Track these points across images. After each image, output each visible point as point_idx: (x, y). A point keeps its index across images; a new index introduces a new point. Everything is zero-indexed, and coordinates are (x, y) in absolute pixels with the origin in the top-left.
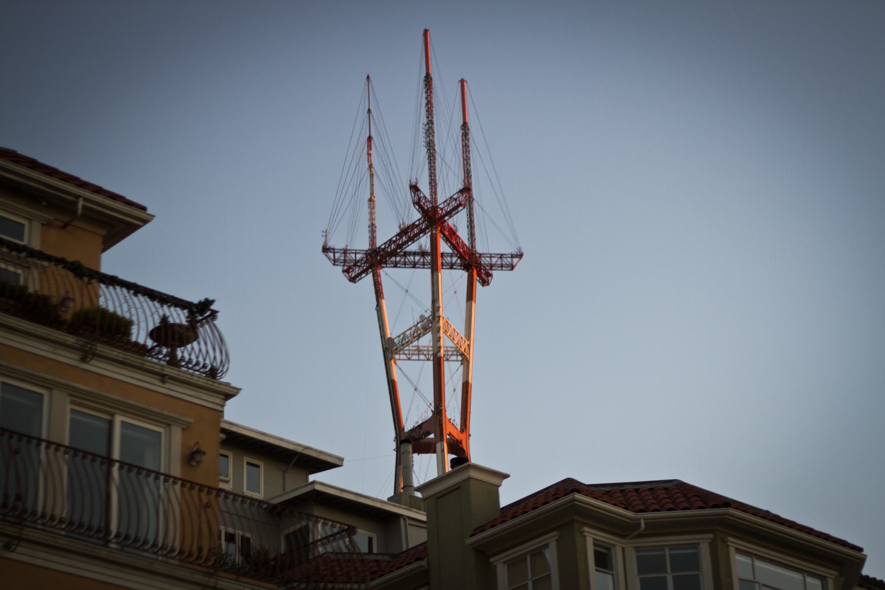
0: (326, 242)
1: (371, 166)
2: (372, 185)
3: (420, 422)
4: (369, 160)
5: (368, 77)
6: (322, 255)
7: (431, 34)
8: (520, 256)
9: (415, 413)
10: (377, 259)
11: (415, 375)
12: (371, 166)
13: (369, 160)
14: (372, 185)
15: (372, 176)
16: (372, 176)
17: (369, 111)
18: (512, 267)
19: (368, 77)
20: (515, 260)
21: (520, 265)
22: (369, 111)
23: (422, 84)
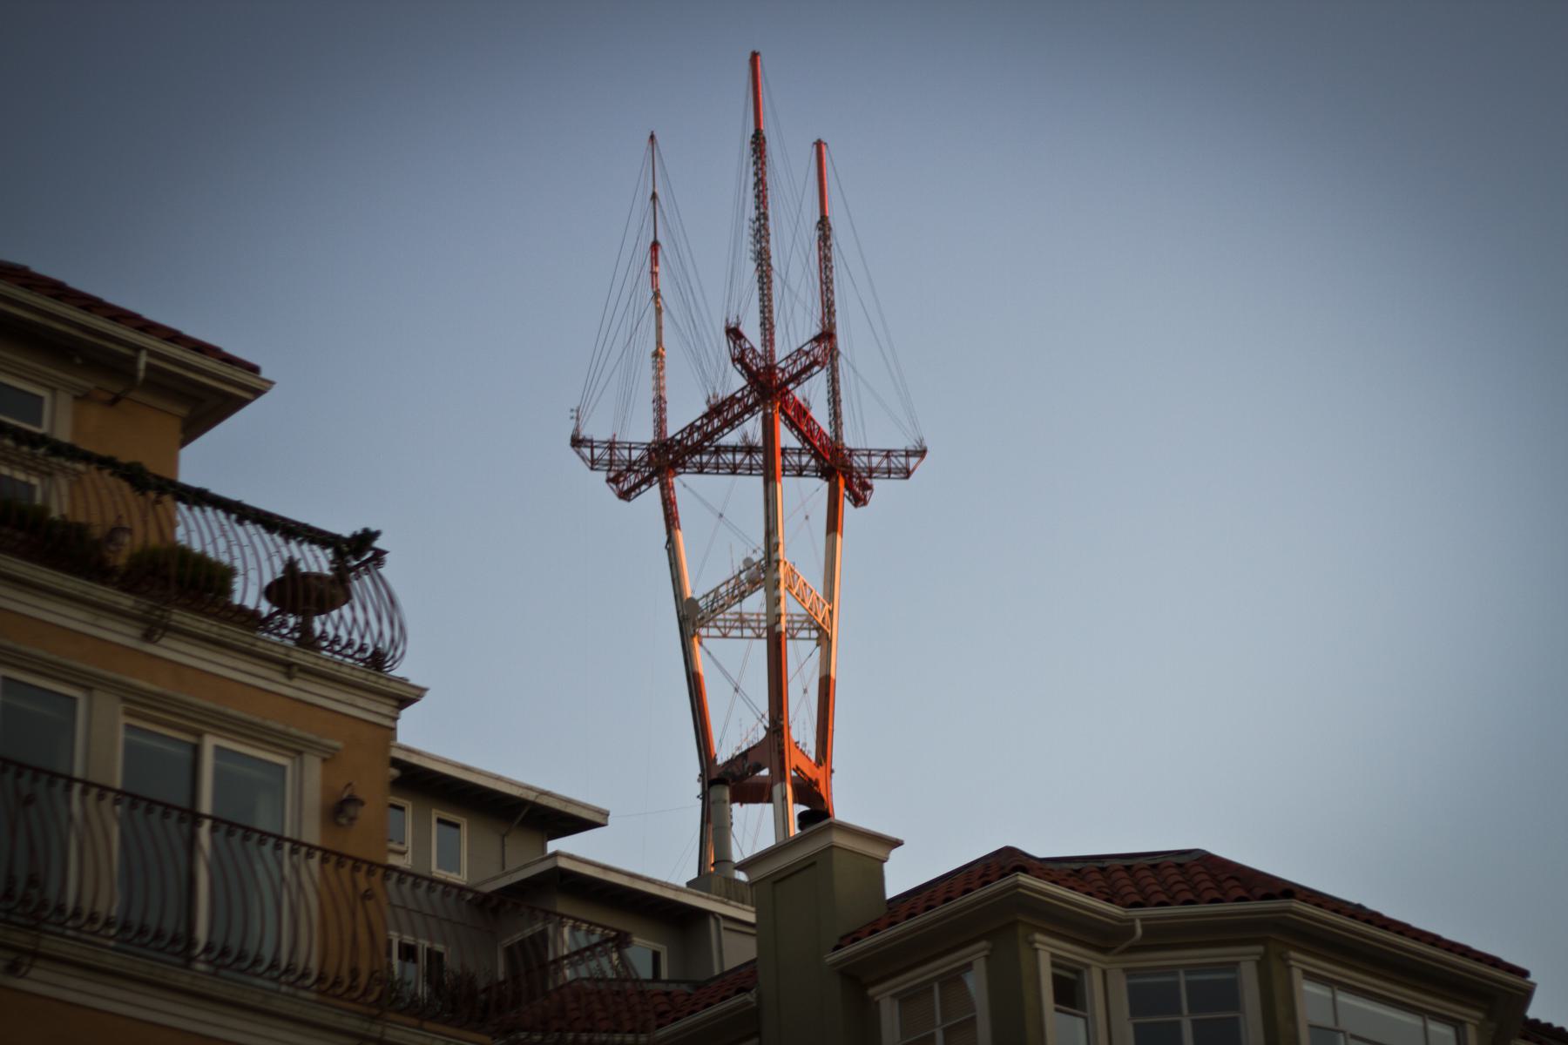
0: (577, 429)
1: (657, 295)
2: (659, 328)
3: (744, 748)
4: (654, 284)
5: (652, 137)
6: (571, 452)
7: (763, 62)
8: (922, 453)
9: (736, 732)
10: (667, 458)
11: (736, 664)
12: (657, 295)
13: (654, 284)
14: (659, 328)
15: (659, 311)
16: (659, 311)
17: (654, 196)
18: (907, 473)
19: (652, 137)
20: (913, 461)
21: (922, 469)
22: (654, 196)
23: (748, 148)
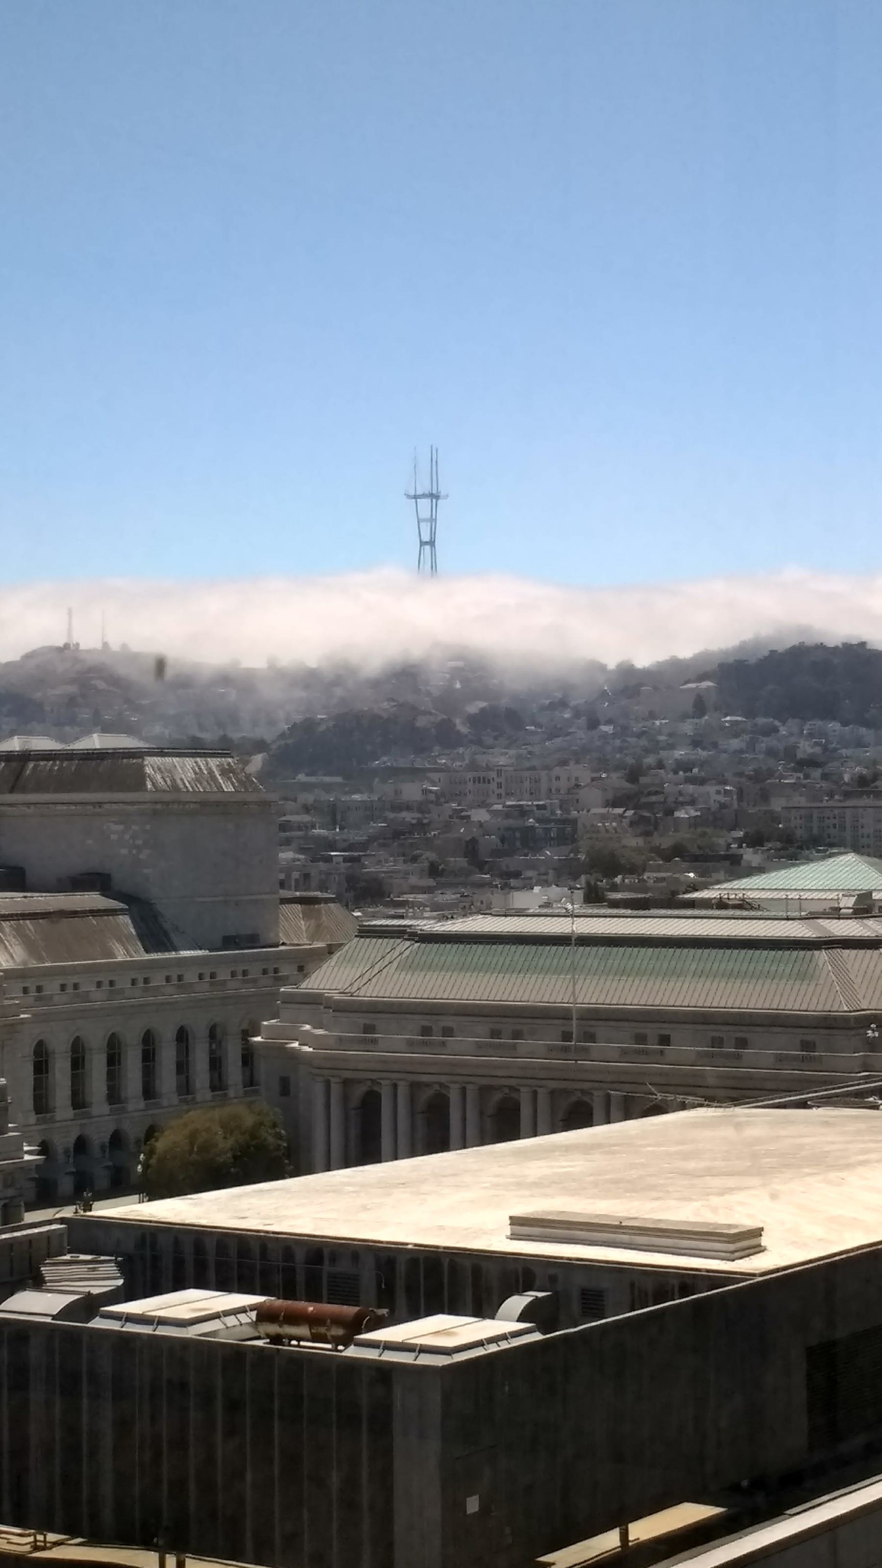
9: (426, 538)
10: (416, 497)
